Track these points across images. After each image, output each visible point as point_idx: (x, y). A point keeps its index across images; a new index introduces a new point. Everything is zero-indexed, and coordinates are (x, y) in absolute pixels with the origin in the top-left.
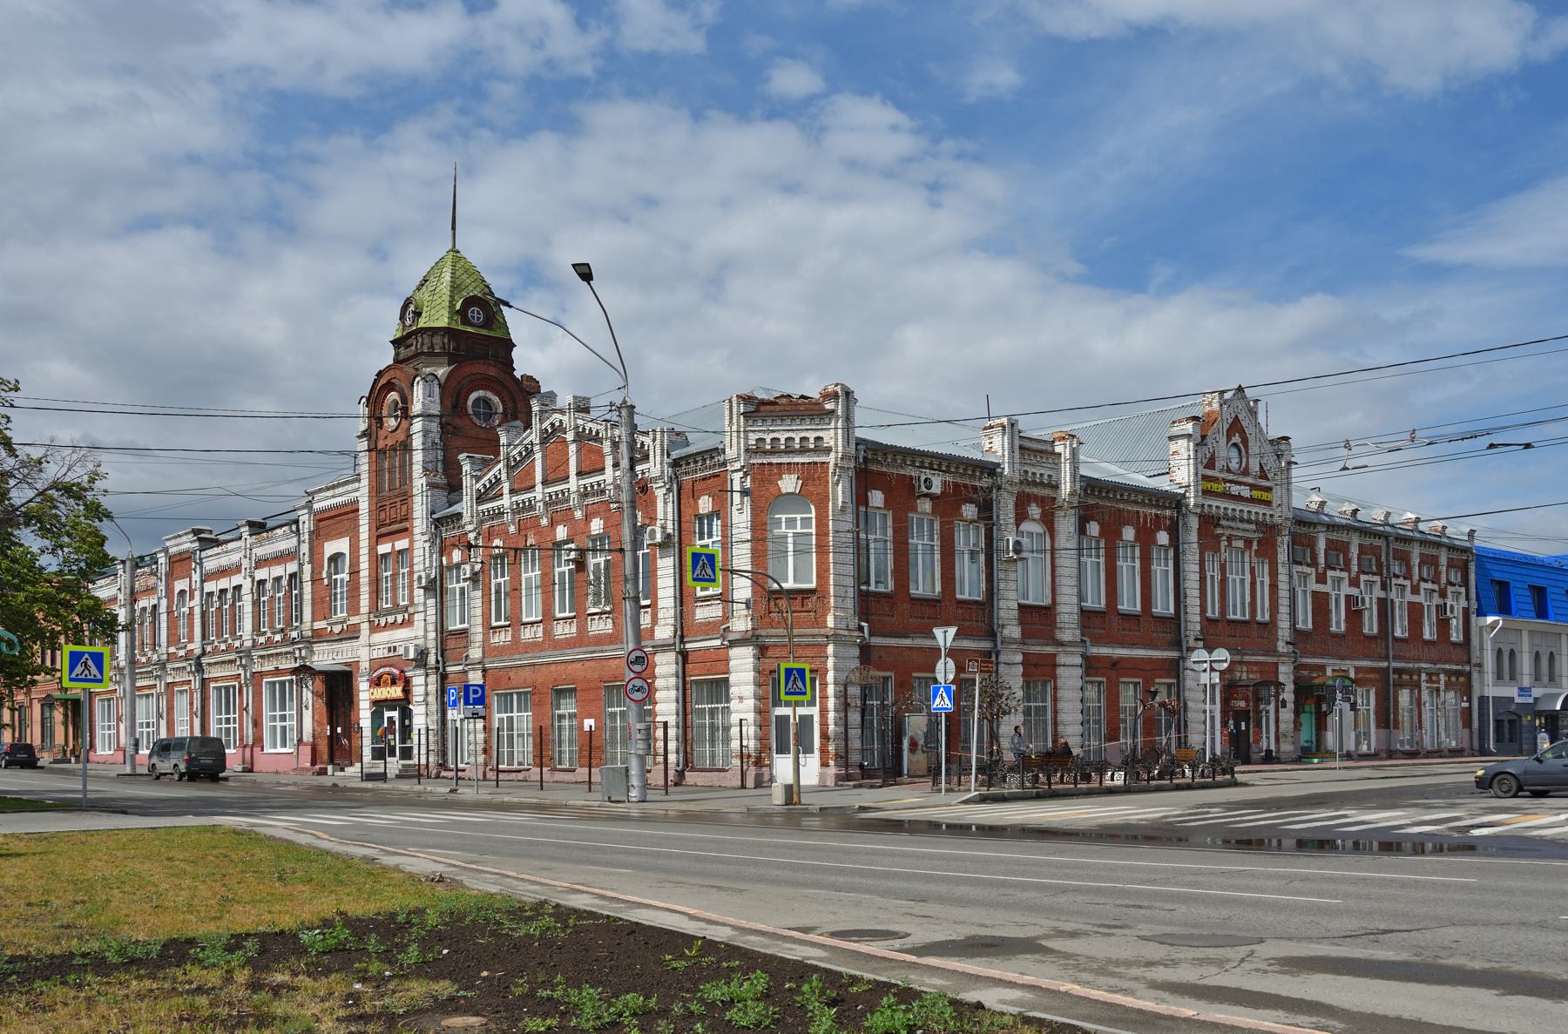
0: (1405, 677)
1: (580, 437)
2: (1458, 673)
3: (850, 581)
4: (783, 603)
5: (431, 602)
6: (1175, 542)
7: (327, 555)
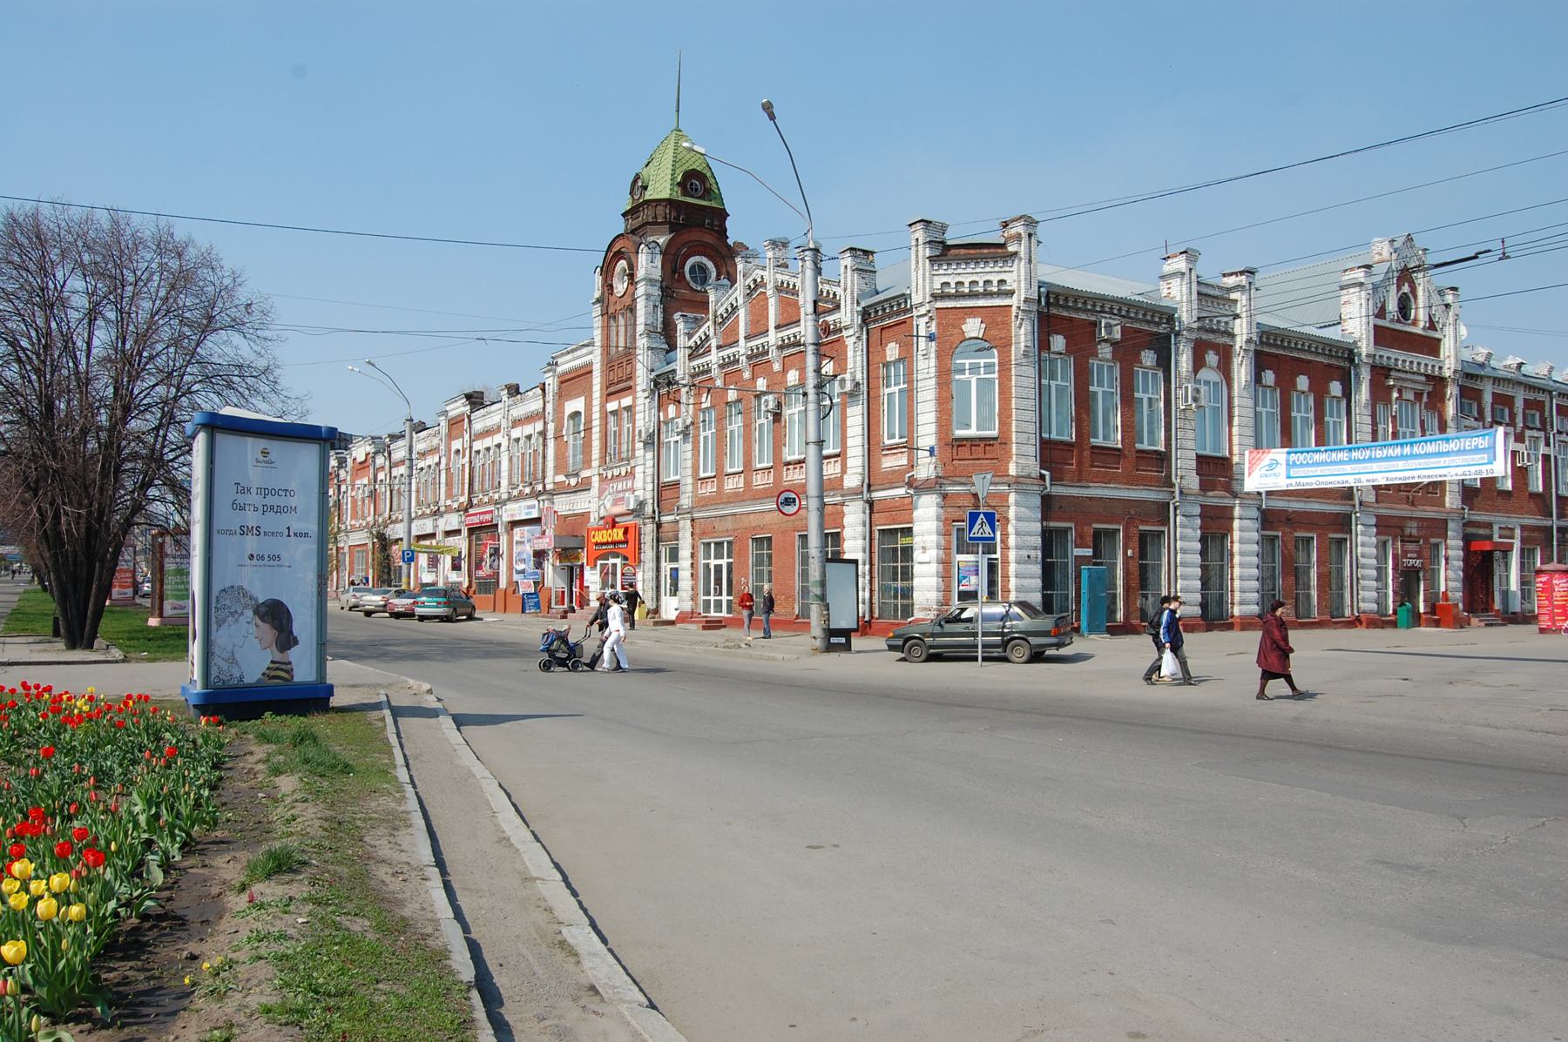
1: (779, 288)
3: (1032, 428)
4: (964, 452)
5: (649, 455)
6: (1347, 394)
7: (567, 413)
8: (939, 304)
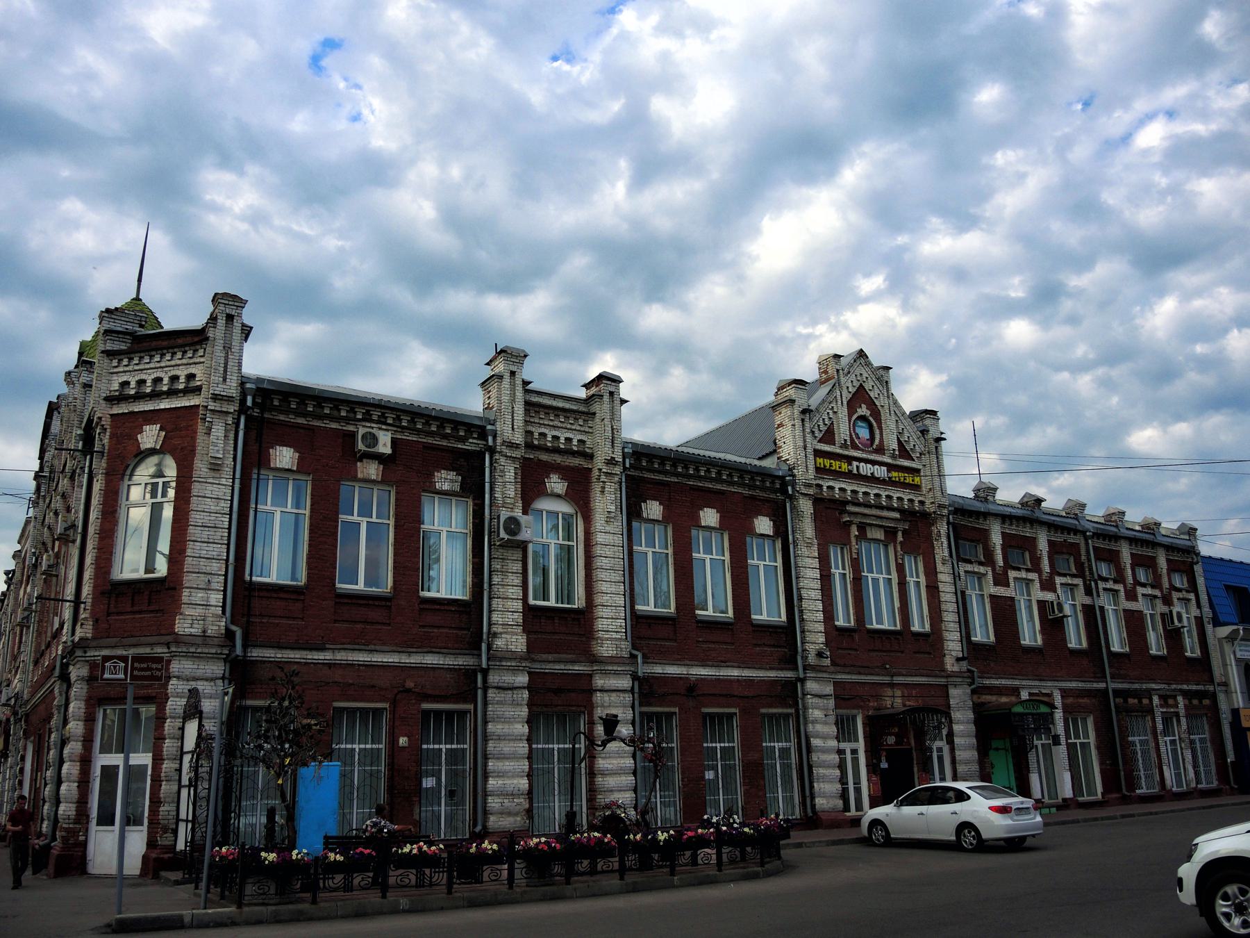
0: (1195, 702)
2: (1201, 695)
6: (781, 531)
8: (117, 410)
